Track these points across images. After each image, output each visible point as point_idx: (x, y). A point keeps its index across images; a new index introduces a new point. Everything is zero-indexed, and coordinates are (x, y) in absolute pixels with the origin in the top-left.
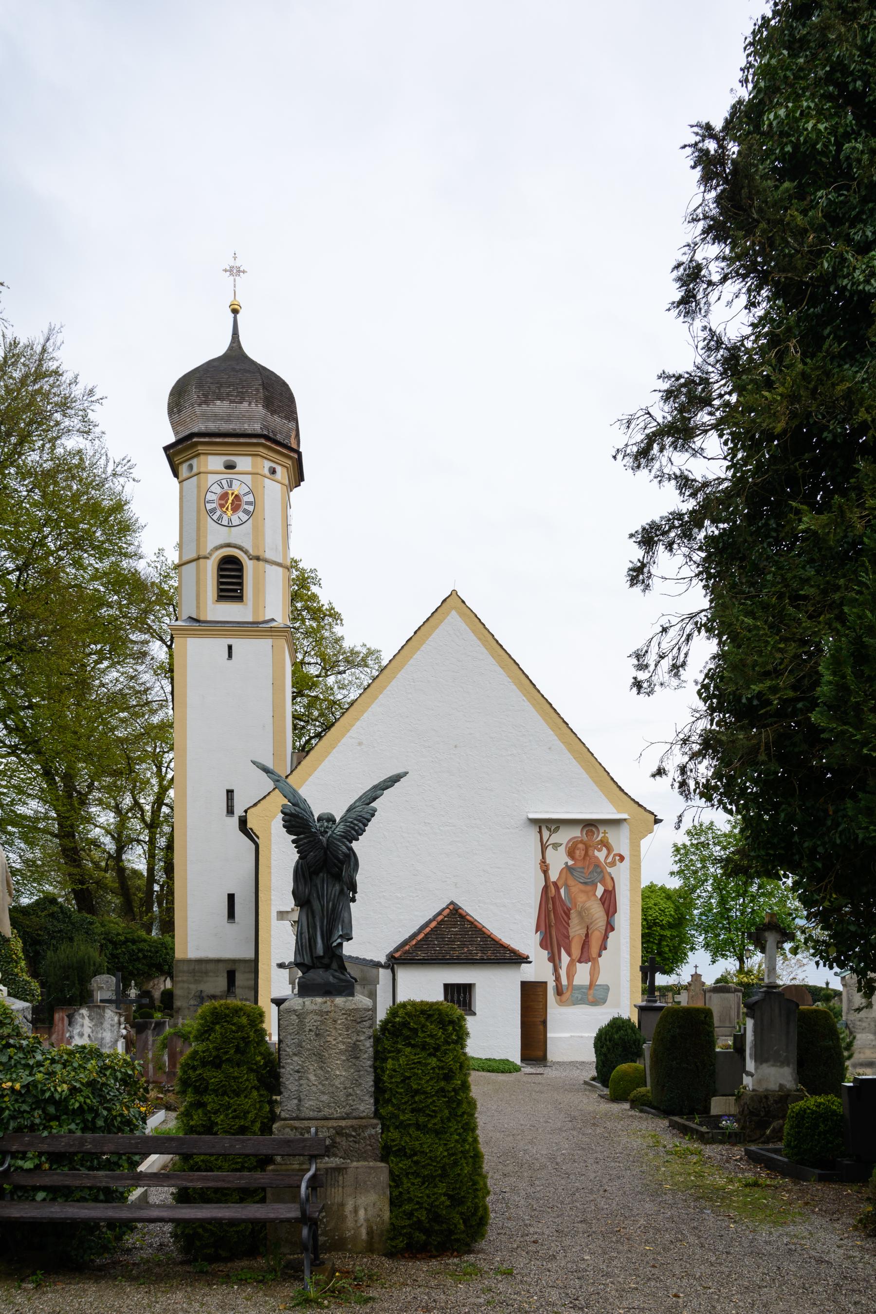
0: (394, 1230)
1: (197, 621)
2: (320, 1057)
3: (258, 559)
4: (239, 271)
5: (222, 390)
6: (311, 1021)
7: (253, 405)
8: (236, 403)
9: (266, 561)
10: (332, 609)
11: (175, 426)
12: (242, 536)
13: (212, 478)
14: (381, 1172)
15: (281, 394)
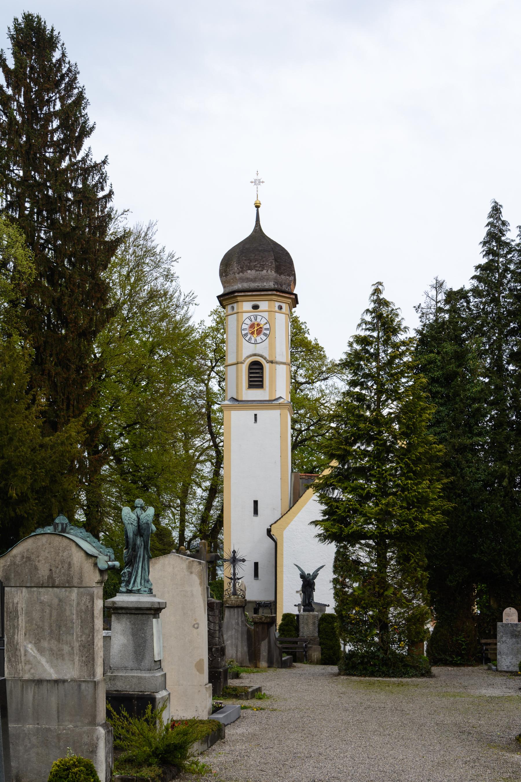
0: (322, 659)
1: (237, 400)
2: (307, 624)
3: (272, 362)
4: (260, 182)
5: (251, 264)
6: (305, 617)
7: (269, 271)
8: (260, 271)
9: (277, 363)
10: (317, 344)
11: (224, 283)
12: (262, 349)
13: (245, 315)
14: (319, 648)
15: (285, 261)
